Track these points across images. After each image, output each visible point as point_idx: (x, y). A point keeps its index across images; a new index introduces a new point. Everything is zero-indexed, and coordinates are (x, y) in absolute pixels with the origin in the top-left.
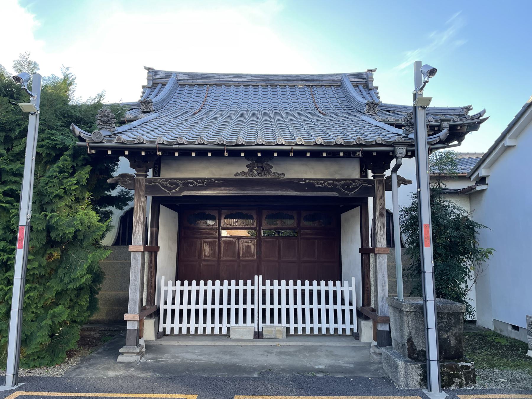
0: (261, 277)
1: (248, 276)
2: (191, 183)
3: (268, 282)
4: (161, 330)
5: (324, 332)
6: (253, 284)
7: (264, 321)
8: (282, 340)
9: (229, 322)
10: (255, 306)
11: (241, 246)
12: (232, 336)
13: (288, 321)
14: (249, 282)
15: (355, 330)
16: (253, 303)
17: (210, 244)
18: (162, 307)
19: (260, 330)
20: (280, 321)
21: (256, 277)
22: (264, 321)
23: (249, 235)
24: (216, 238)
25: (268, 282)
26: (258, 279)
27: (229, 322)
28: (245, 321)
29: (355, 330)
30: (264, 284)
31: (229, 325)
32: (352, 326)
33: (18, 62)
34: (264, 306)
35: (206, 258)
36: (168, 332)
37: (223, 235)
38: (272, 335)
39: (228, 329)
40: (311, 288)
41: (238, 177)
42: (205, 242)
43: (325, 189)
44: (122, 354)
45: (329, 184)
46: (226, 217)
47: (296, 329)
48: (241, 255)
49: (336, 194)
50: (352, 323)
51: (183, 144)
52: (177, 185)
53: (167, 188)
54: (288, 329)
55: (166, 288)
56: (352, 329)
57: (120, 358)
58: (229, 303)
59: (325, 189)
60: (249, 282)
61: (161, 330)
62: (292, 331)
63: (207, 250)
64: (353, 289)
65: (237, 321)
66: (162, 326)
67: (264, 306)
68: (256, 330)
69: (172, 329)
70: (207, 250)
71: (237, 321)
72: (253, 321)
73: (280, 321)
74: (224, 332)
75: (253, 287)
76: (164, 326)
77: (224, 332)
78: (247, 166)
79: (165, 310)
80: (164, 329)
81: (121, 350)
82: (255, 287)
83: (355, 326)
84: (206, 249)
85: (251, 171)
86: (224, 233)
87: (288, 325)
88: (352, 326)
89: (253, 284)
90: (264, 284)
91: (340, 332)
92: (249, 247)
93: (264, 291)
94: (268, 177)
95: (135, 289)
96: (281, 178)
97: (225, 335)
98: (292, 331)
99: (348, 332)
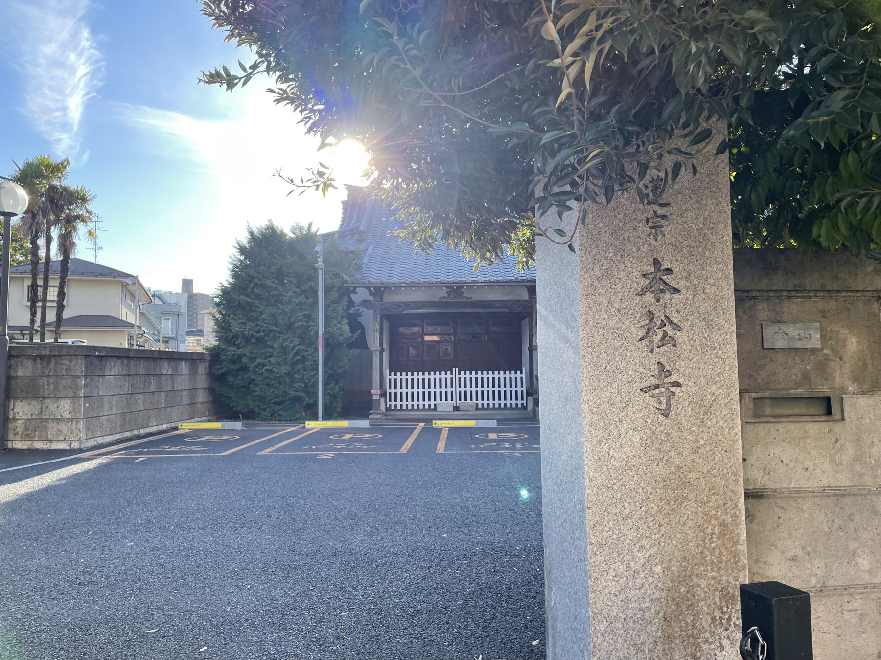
0: (457, 369)
1: (447, 368)
2: (410, 305)
3: (462, 372)
4: (388, 406)
5: (503, 406)
6: (452, 374)
7: (460, 400)
8: (473, 411)
9: (435, 400)
10: (454, 389)
11: (440, 348)
12: (438, 409)
13: (477, 399)
14: (449, 373)
15: (525, 405)
16: (452, 387)
17: (415, 347)
18: (388, 391)
19: (457, 405)
20: (471, 399)
21: (454, 369)
22: (460, 400)
23: (438, 339)
24: (420, 342)
25: (462, 372)
26: (455, 370)
27: (435, 400)
28: (446, 400)
29: (525, 405)
30: (460, 374)
31: (435, 403)
32: (523, 402)
33: (293, 227)
34: (460, 389)
35: (413, 359)
36: (393, 407)
37: (426, 339)
38: (466, 408)
39: (435, 405)
40: (493, 376)
41: (442, 300)
42: (412, 346)
43: (499, 307)
44: (371, 414)
45: (503, 304)
46: (429, 324)
47: (483, 405)
48: (440, 356)
49: (507, 311)
50: (522, 399)
51: (408, 283)
52: (401, 307)
53: (394, 309)
54: (477, 405)
55: (390, 377)
56: (522, 404)
57: (370, 417)
58: (435, 392)
59: (499, 307)
60: (449, 373)
61: (388, 406)
62: (480, 406)
63: (413, 352)
64: (524, 376)
65: (441, 400)
66: (388, 403)
67: (460, 389)
68: (455, 405)
69: (396, 406)
70: (413, 352)
71: (441, 400)
72: (452, 400)
73: (471, 399)
74: (432, 407)
75: (452, 376)
76: (390, 403)
77: (432, 407)
78: (447, 293)
79: (390, 393)
80: (390, 405)
81: (370, 412)
82: (453, 376)
83: (524, 402)
84: (412, 351)
85: (449, 296)
86: (427, 338)
87: (477, 402)
88: (523, 402)
89: (452, 374)
90: (460, 374)
91: (514, 406)
92: (447, 349)
93: (460, 379)
94: (461, 300)
95: (377, 375)
96: (470, 300)
97: (433, 409)
98: (480, 406)
99: (520, 406)
